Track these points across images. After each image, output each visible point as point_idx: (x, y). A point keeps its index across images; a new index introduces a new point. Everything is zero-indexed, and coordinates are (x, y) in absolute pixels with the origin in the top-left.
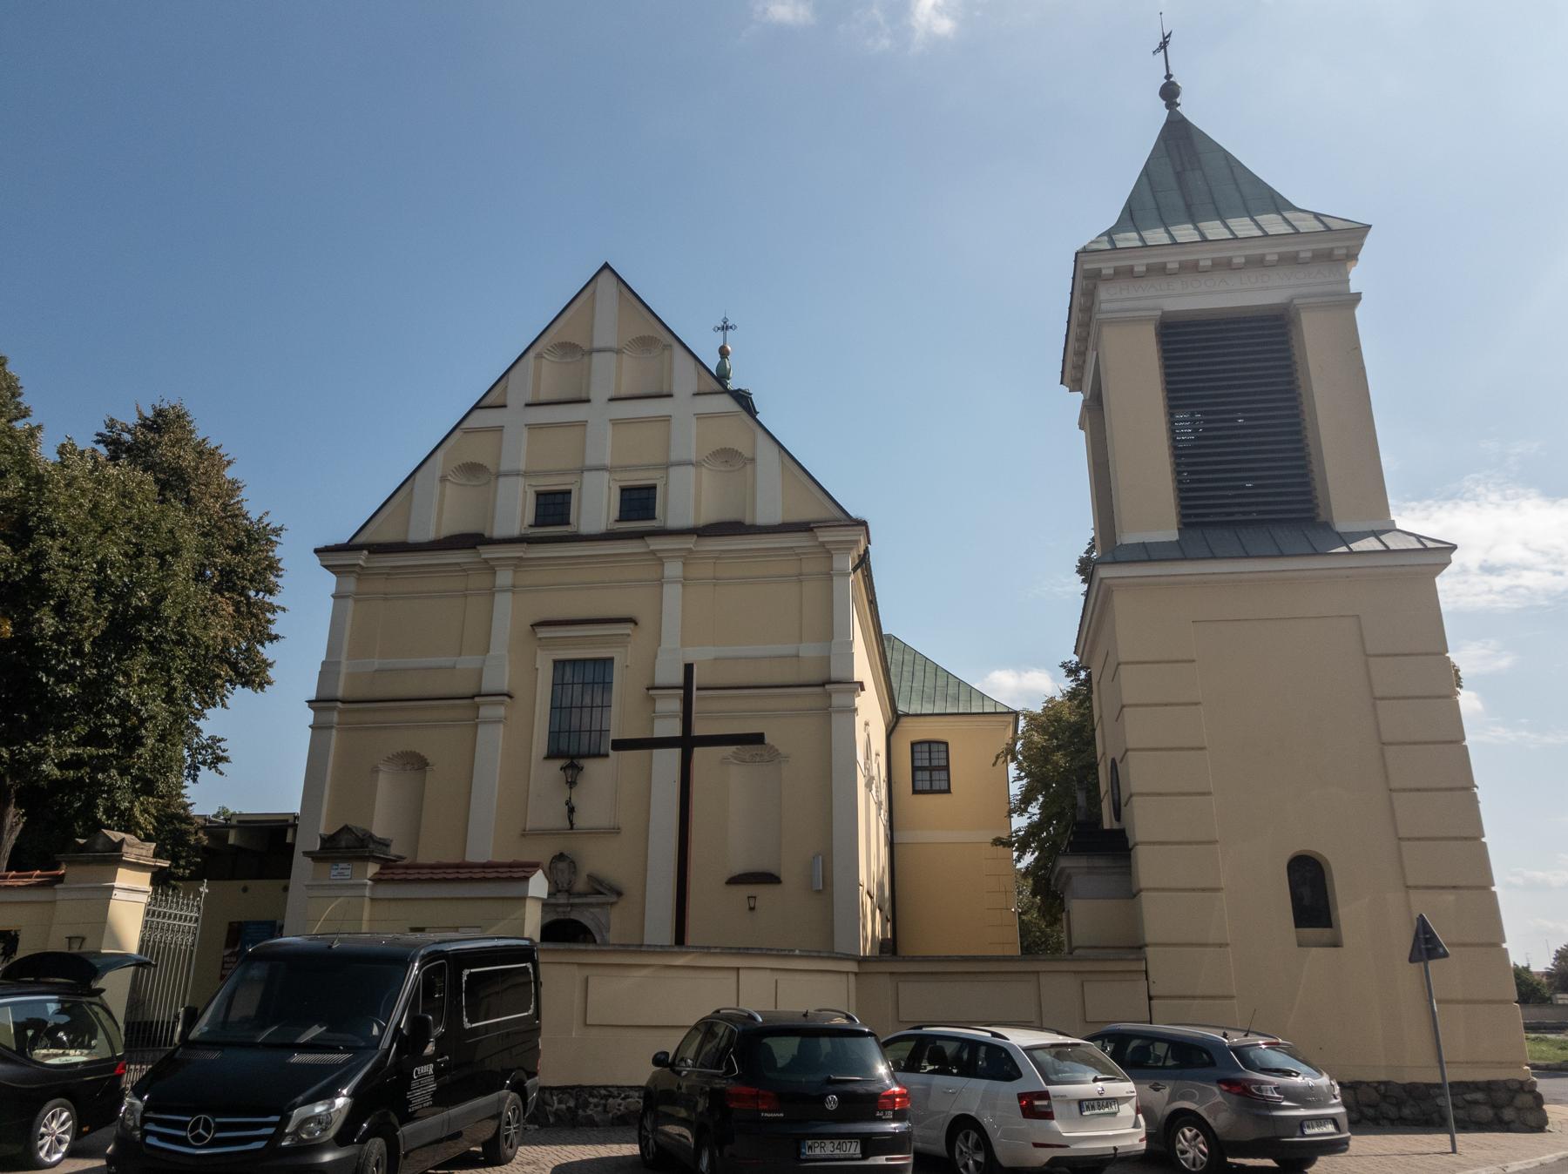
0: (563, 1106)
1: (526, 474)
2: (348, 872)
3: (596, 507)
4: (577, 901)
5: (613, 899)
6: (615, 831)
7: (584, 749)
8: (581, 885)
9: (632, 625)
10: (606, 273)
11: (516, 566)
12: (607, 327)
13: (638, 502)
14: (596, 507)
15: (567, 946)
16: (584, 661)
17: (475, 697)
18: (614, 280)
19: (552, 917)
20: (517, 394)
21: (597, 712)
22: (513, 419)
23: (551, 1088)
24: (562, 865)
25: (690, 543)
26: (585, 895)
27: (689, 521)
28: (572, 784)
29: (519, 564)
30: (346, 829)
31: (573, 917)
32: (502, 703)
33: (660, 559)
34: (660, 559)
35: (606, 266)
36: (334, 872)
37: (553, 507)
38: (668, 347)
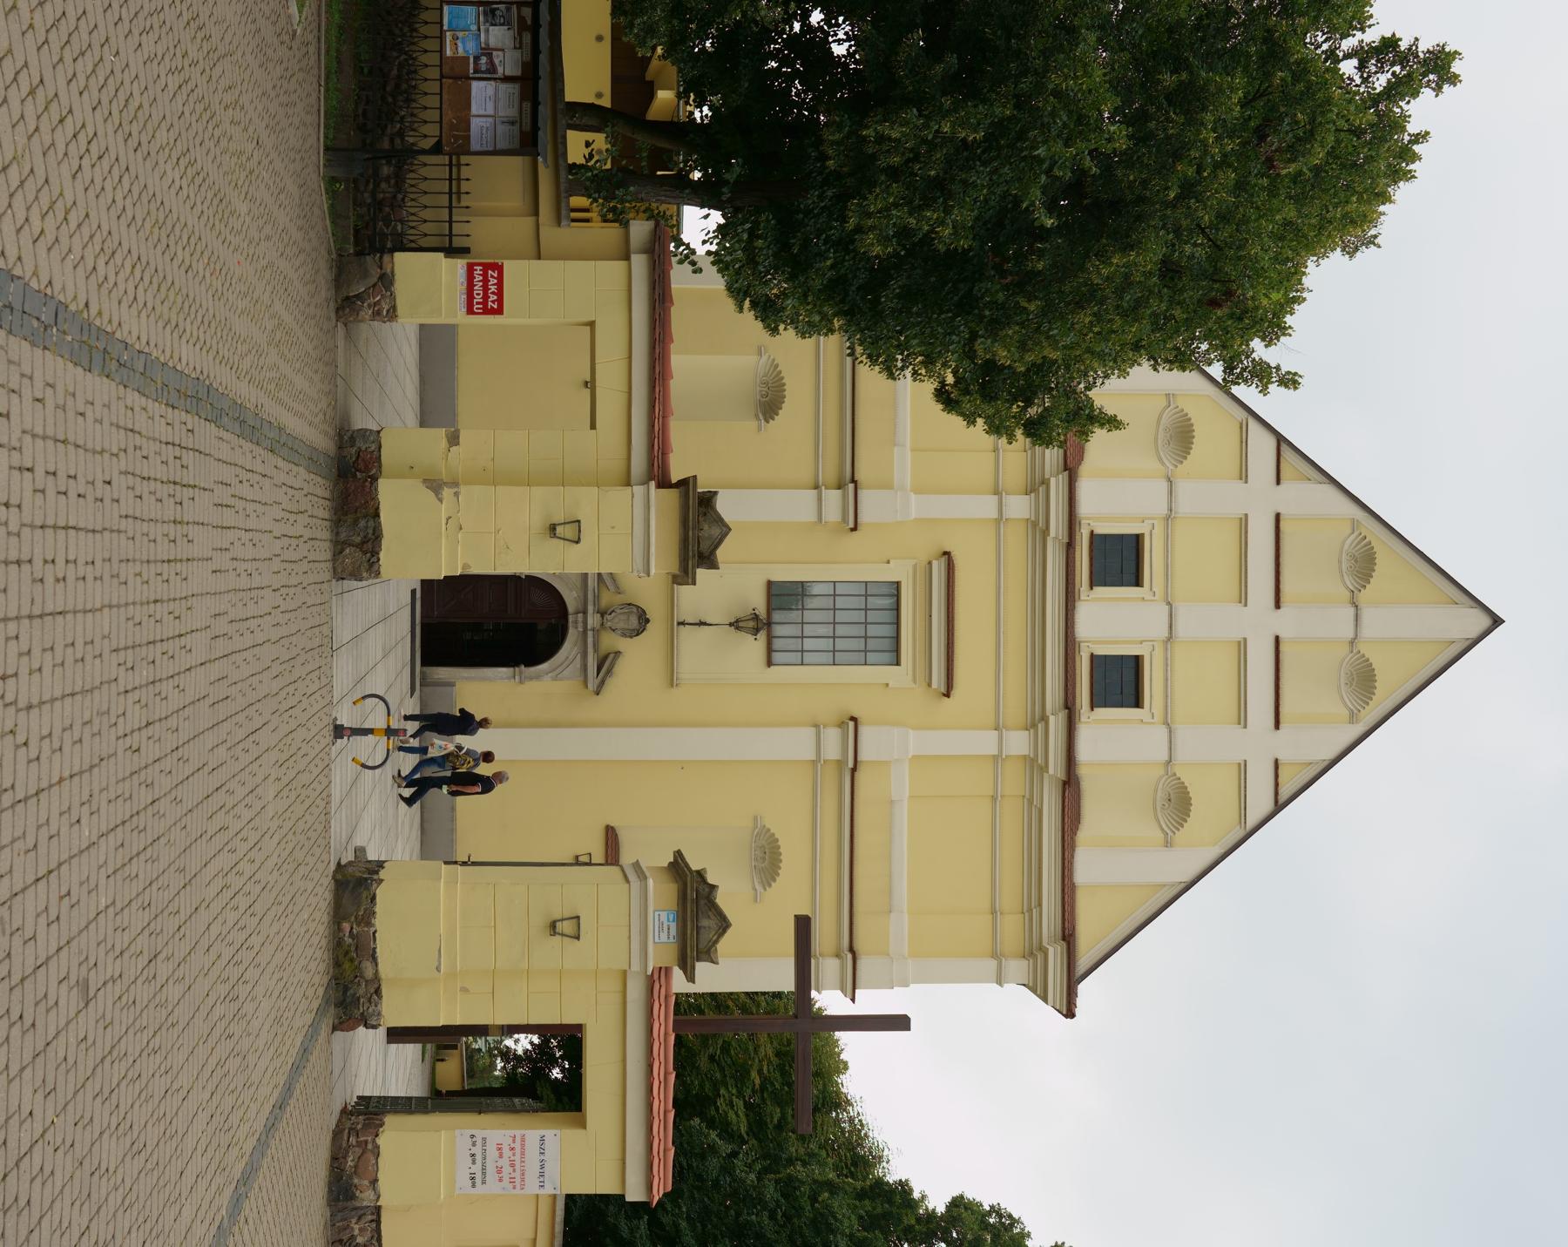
0: (356, 1232)
1: (1169, 518)
2: (664, 937)
3: (1110, 621)
4: (590, 640)
5: (592, 685)
6: (672, 680)
7: (777, 644)
8: (610, 641)
9: (943, 690)
10: (1486, 621)
11: (1035, 524)
12: (1398, 621)
13: (1120, 681)
14: (1110, 621)
15: (559, 1228)
16: (898, 623)
17: (850, 481)
18: (1474, 634)
19: (571, 599)
20: (1298, 497)
21: (826, 644)
22: (1260, 498)
23: (378, 1222)
24: (634, 622)
25: (1056, 768)
26: (596, 649)
27: (1084, 752)
28: (736, 625)
29: (1038, 529)
30: (724, 925)
31: (571, 631)
32: (845, 519)
33: (1034, 726)
34: (1034, 726)
35: (1497, 621)
36: (664, 916)
37: (1120, 560)
38: (1353, 718)
